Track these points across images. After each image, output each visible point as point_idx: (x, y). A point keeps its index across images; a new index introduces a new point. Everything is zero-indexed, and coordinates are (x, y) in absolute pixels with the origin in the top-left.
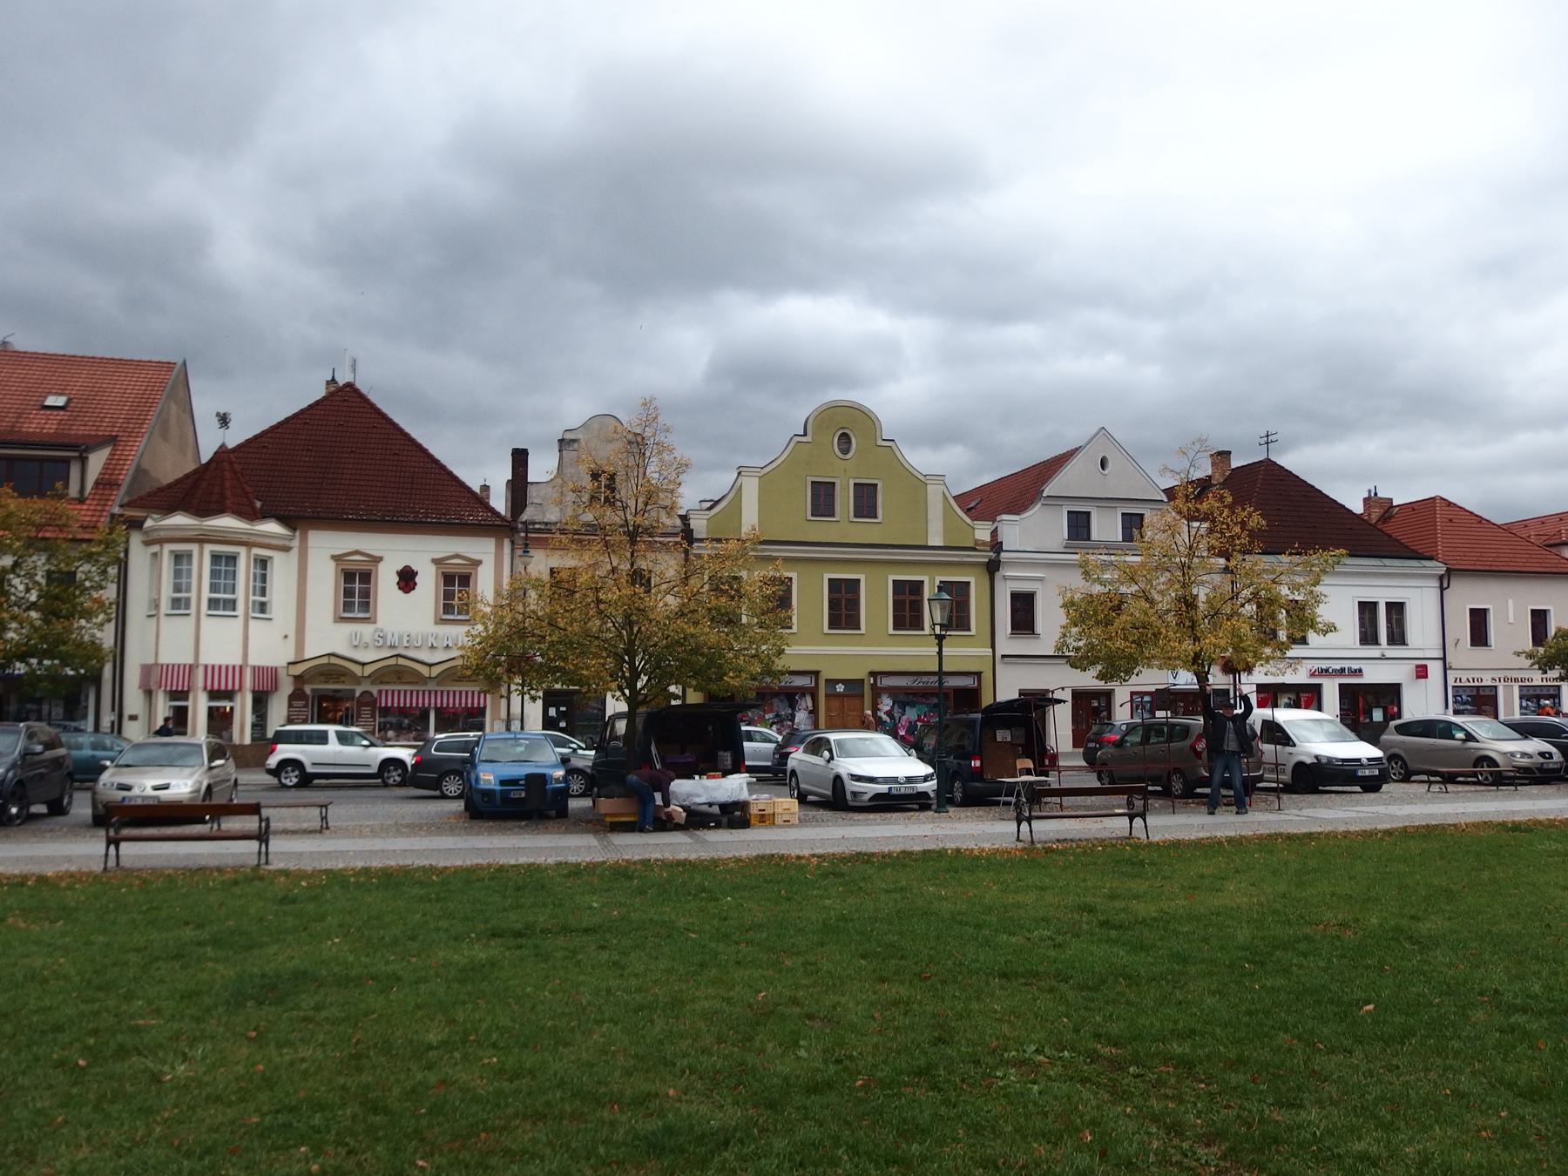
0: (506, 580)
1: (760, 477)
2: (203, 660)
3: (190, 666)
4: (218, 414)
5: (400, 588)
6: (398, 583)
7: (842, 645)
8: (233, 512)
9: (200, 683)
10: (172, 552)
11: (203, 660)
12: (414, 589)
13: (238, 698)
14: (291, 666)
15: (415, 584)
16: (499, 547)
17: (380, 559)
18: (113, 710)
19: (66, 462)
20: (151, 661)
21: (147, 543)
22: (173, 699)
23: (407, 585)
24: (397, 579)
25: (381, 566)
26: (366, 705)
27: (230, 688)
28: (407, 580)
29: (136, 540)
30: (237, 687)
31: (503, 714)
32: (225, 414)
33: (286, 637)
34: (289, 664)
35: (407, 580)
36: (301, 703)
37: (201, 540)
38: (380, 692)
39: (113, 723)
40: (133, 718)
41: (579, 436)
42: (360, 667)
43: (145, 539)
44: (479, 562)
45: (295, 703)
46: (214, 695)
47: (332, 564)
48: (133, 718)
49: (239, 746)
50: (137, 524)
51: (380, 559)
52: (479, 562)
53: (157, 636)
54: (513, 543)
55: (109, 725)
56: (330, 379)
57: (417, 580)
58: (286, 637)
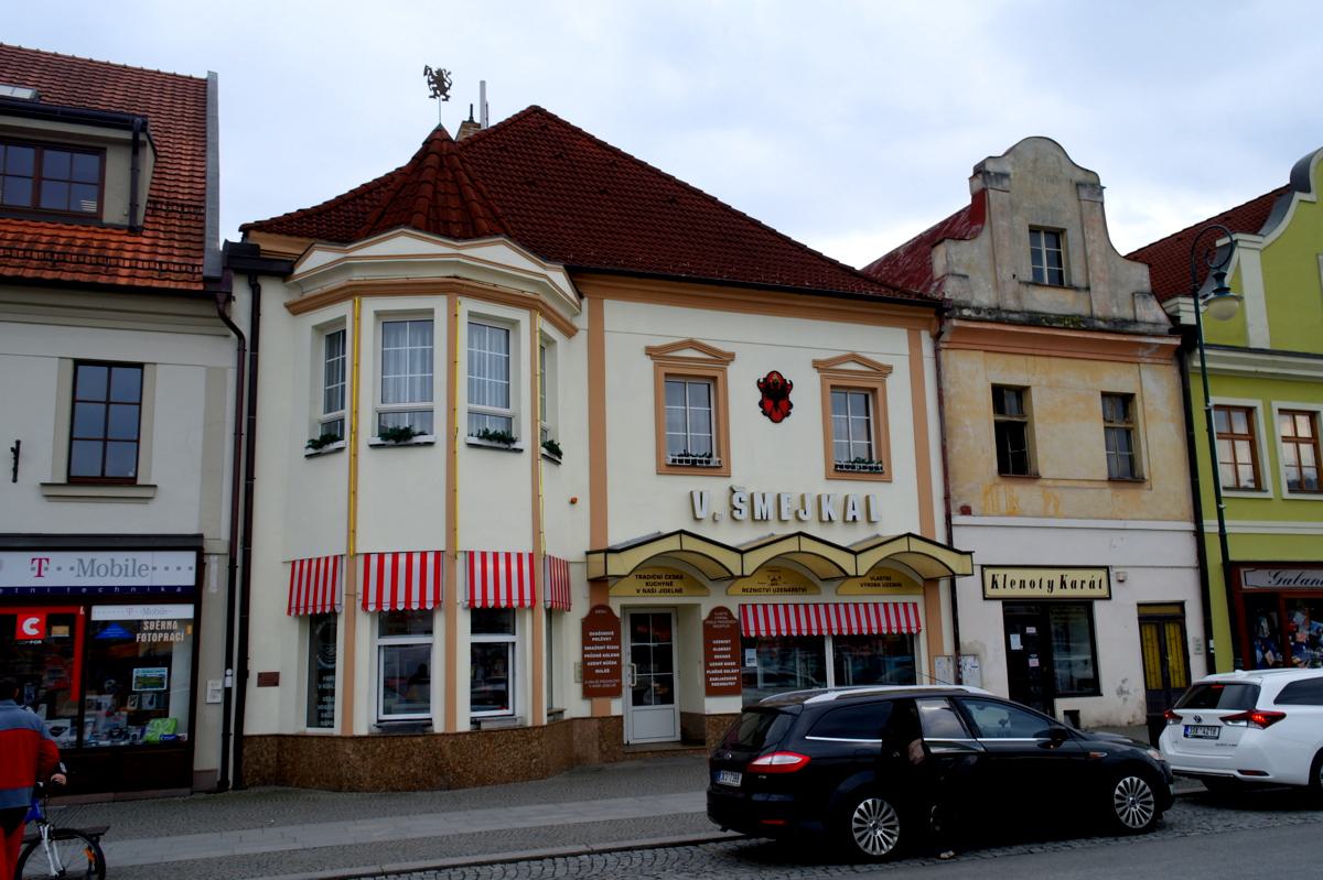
0: (1162, 361)
1: (1261, 251)
2: (464, 544)
3: (438, 554)
4: (427, 70)
5: (764, 413)
6: (761, 404)
7: (1286, 520)
8: (510, 237)
9: (461, 596)
10: (378, 314)
11: (464, 544)
12: (788, 414)
13: (439, 623)
14: (591, 556)
15: (791, 406)
16: (915, 344)
17: (731, 357)
18: (229, 665)
19: (98, 149)
20: (334, 546)
21: (296, 309)
22: (384, 632)
23: (776, 406)
24: (758, 396)
25: (732, 369)
26: (722, 634)
27: (503, 604)
28: (775, 397)
29: (274, 296)
30: (515, 603)
31: (948, 648)
32: (440, 72)
33: (573, 501)
34: (588, 553)
35: (775, 397)
36: (607, 635)
37: (452, 288)
38: (744, 607)
39: (228, 691)
40: (270, 679)
41: (1008, 169)
42: (737, 556)
43: (295, 297)
44: (889, 369)
45: (596, 635)
46: (394, 622)
47: (649, 364)
48: (270, 679)
49: (534, 728)
50: (282, 270)
51: (731, 357)
52: (889, 369)
53: (353, 493)
54: (937, 337)
55: (219, 698)
56: (467, 119)
57: (792, 397)
58: (573, 501)
